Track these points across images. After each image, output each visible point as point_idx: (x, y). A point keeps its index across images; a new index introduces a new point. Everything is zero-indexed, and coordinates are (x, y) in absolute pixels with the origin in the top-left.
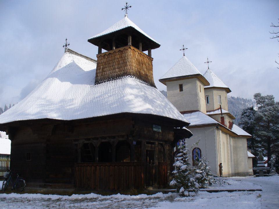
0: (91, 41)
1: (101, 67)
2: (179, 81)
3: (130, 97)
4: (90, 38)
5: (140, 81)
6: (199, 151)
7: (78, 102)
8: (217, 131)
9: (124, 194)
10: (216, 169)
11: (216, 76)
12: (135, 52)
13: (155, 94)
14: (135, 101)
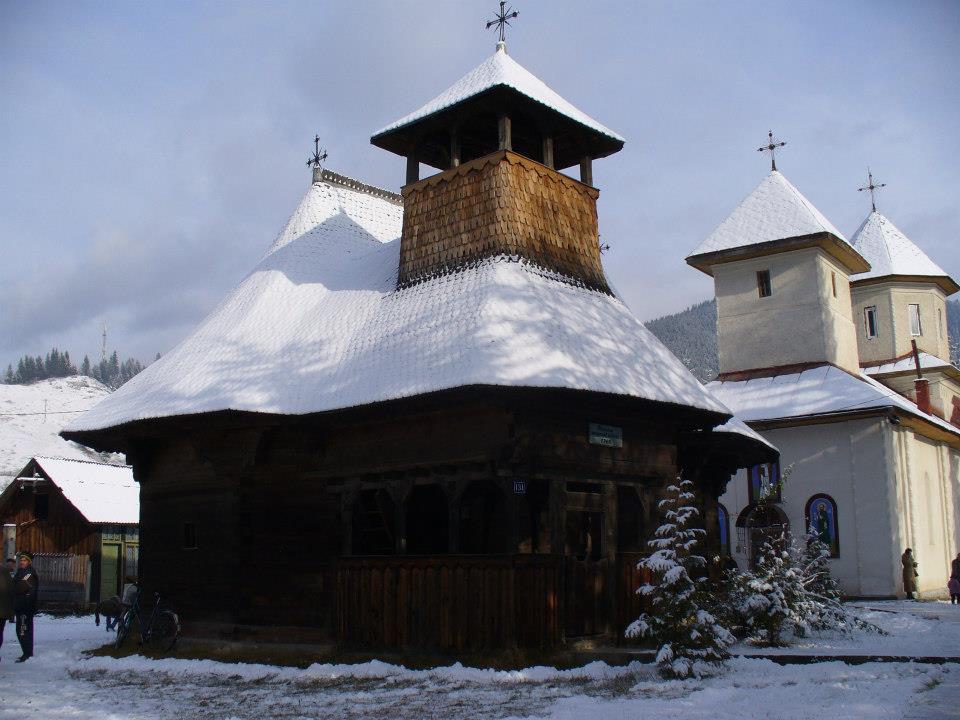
0: (381, 141)
1: (416, 228)
2: (757, 260)
3: (498, 331)
4: (378, 133)
5: (544, 273)
6: (829, 507)
7: (336, 353)
8: (895, 434)
9: (473, 666)
10: (892, 569)
11: (901, 234)
12: (526, 174)
13: (598, 317)
14: (518, 341)
